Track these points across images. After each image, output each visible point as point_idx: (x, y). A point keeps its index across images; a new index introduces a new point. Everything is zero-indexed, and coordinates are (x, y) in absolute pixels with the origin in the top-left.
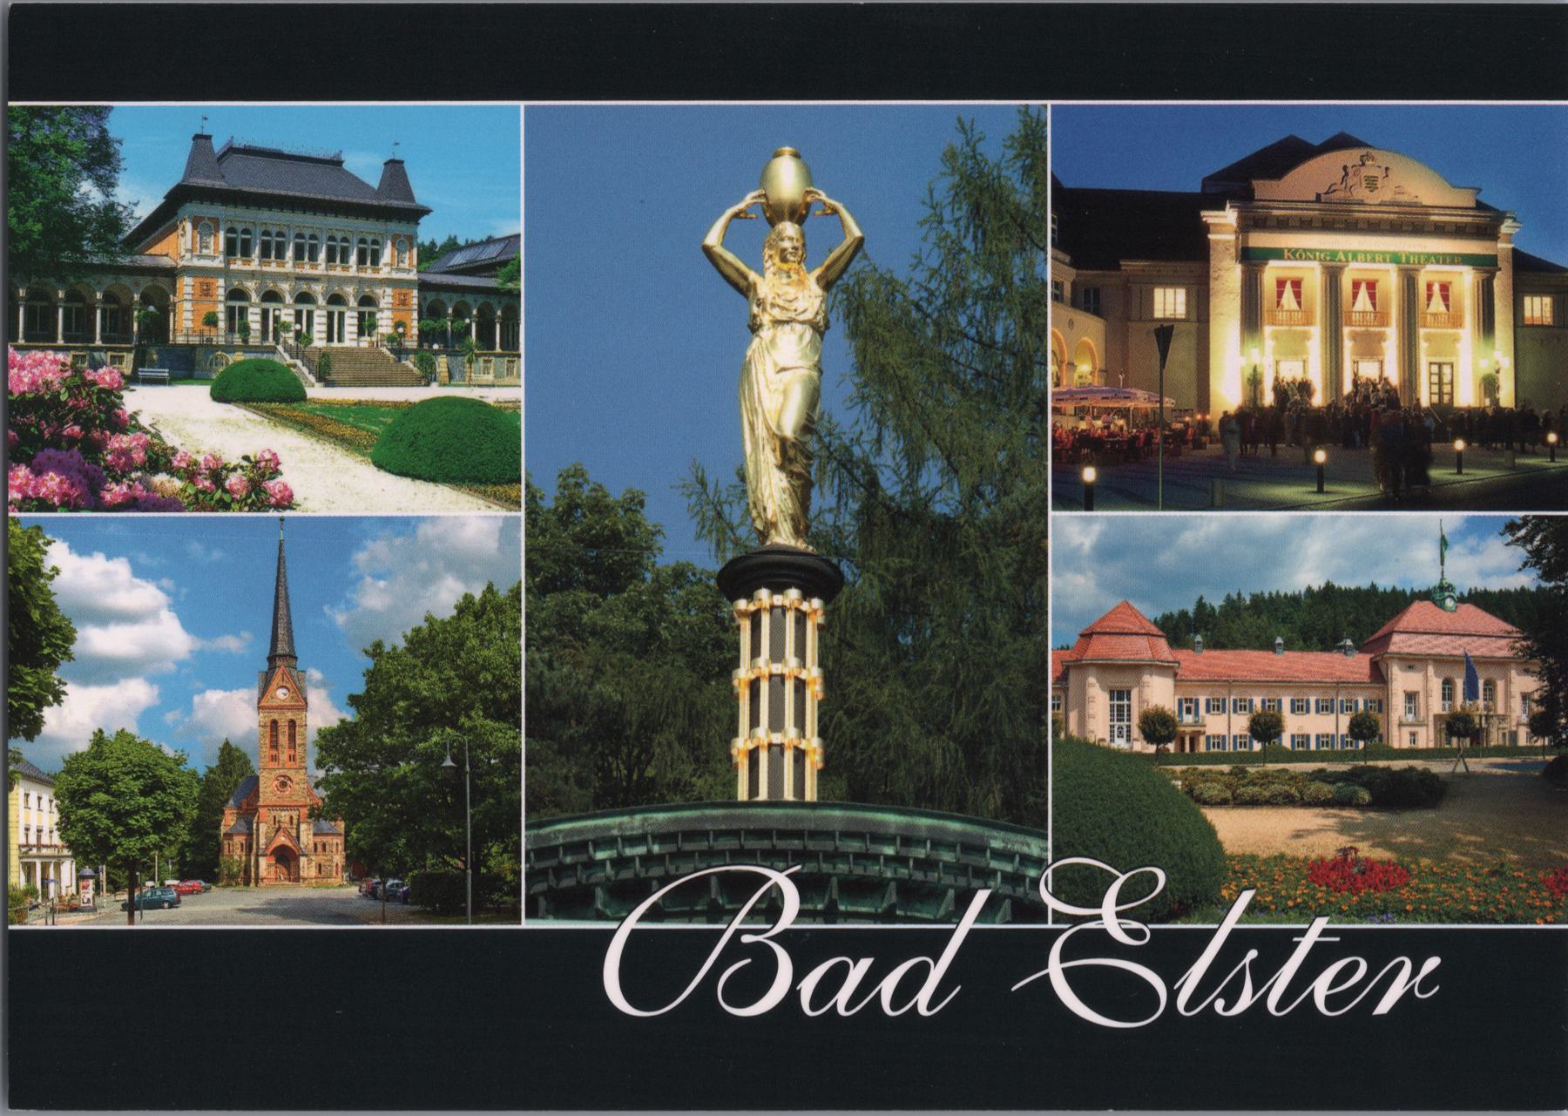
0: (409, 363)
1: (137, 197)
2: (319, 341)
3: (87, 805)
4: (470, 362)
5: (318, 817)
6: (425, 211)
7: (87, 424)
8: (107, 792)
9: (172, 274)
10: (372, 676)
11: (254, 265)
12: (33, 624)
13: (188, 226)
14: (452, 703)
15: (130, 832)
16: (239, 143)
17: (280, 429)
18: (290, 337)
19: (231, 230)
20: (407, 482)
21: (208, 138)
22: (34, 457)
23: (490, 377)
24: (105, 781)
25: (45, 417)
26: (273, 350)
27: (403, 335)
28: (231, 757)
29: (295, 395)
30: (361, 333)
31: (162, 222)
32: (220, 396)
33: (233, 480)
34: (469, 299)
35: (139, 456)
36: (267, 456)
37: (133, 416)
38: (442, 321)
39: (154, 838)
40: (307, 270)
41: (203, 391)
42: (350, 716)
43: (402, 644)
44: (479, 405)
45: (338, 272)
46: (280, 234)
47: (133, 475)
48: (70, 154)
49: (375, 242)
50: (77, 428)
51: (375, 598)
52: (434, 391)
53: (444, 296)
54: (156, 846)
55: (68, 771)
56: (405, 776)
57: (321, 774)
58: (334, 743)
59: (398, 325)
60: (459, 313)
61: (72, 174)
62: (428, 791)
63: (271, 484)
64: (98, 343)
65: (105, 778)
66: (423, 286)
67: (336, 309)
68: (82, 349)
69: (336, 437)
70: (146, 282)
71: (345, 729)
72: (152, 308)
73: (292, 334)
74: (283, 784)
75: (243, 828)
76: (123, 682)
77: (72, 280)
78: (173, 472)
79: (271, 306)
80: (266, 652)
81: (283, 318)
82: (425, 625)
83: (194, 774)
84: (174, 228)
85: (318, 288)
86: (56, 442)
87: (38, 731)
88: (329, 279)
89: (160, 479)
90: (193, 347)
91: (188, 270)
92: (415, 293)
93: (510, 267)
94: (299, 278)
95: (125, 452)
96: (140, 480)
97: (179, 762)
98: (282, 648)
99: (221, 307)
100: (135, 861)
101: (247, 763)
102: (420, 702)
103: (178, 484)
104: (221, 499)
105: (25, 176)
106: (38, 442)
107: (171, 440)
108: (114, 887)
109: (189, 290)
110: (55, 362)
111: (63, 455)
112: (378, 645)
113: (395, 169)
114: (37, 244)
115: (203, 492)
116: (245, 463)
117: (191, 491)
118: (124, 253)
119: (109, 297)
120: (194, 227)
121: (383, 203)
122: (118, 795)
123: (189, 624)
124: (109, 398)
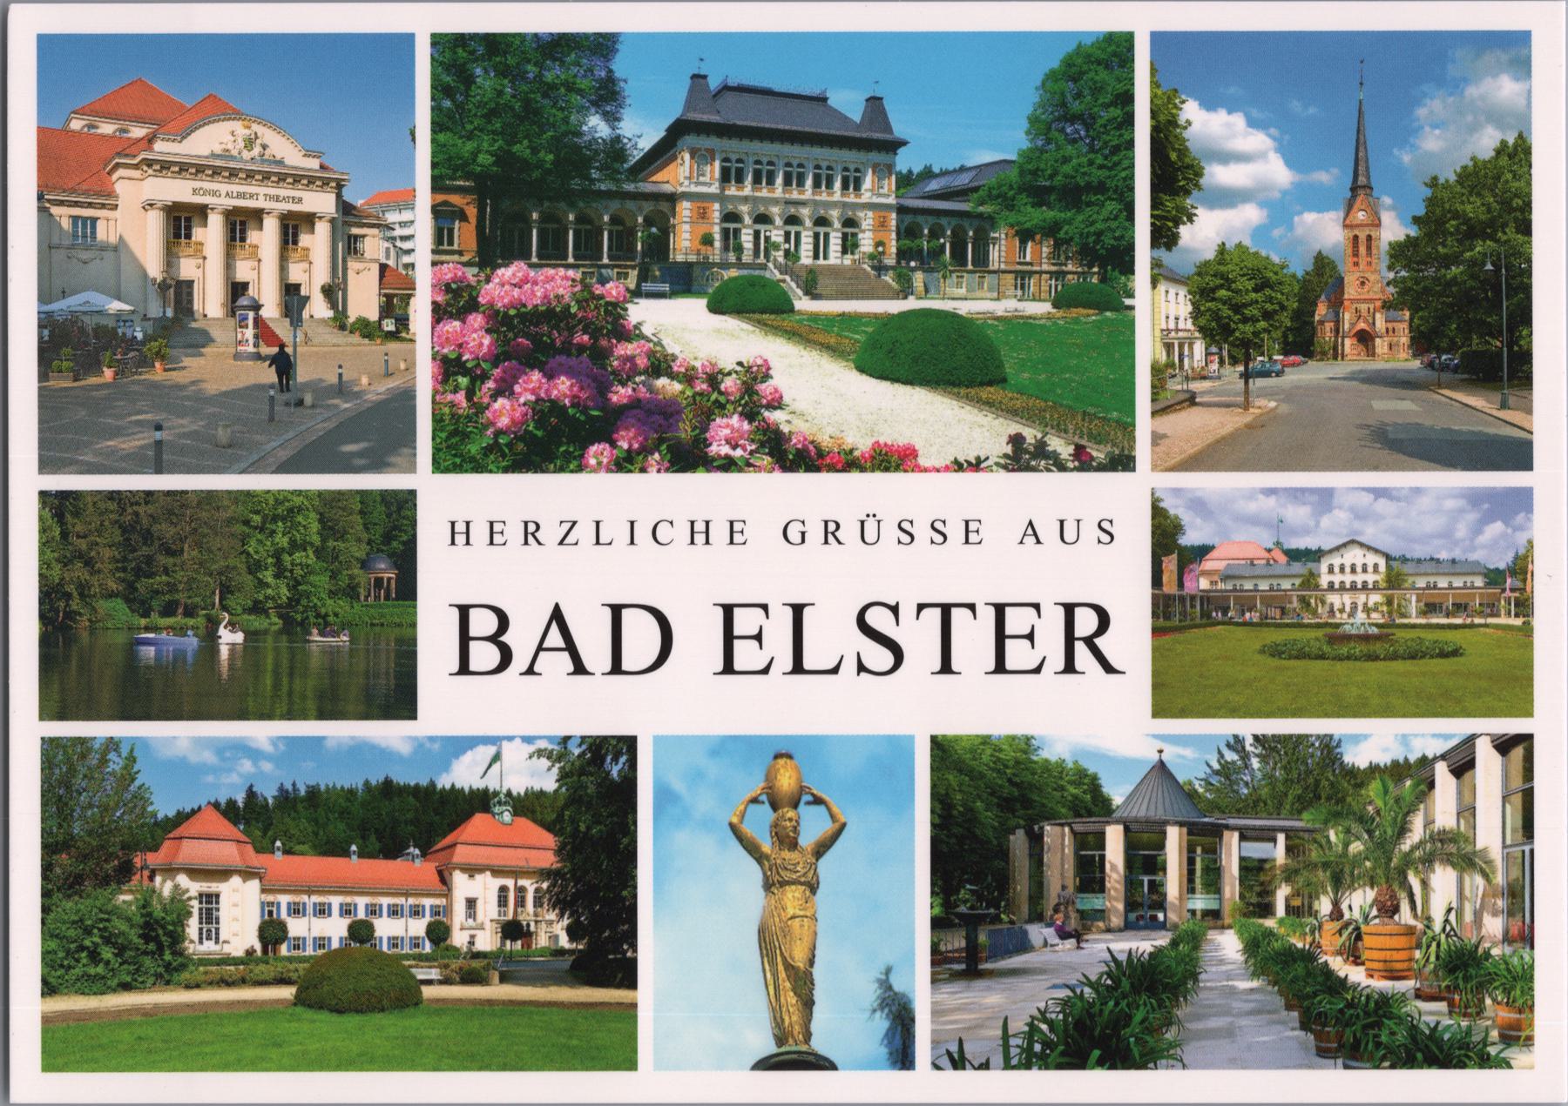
0: (888, 278)
1: (641, 130)
2: (806, 258)
3: (1214, 299)
4: (945, 277)
5: (1388, 309)
6: (903, 143)
7: (595, 334)
8: (1229, 289)
9: (672, 199)
10: (1431, 202)
11: (747, 190)
12: (1173, 163)
13: (687, 156)
14: (1492, 223)
15: (1245, 320)
16: (732, 82)
17: (770, 338)
18: (779, 256)
19: (726, 160)
20: (886, 385)
21: (705, 77)
22: (545, 363)
23: (962, 291)
24: (1227, 282)
25: (556, 327)
26: (764, 267)
27: (883, 253)
28: (1322, 263)
29: (783, 306)
30: (844, 251)
31: (662, 152)
32: (716, 308)
33: (729, 384)
34: (944, 221)
35: (642, 362)
36: (759, 362)
37: (637, 327)
38: (917, 242)
39: (1262, 324)
40: (795, 195)
41: (700, 304)
42: (1413, 232)
43: (1453, 178)
44: (954, 316)
45: (824, 197)
46: (770, 163)
47: (637, 379)
48: (580, 92)
49: (857, 170)
50: (586, 338)
51: (1432, 142)
52: (911, 304)
53: (920, 219)
54: (1265, 330)
55: (1199, 274)
56: (1455, 277)
57: (1391, 275)
58: (1399, 252)
59: (878, 244)
60: (935, 234)
61: (582, 110)
62: (1473, 288)
63: (763, 386)
64: (606, 261)
65: (1227, 279)
66: (901, 210)
67: (822, 230)
68: (591, 266)
69: (822, 345)
70: (648, 207)
71: (1410, 243)
72: (654, 230)
73: (781, 253)
74: (1363, 283)
75: (1331, 316)
76: (1241, 207)
77: (581, 204)
78: (673, 376)
79: (762, 227)
80: (1349, 184)
81: (773, 239)
82: (1471, 164)
83: (1294, 276)
84: (674, 158)
85: (805, 212)
86: (567, 349)
87: (1175, 243)
88: (815, 203)
89: (662, 382)
90: (689, 265)
91: (687, 196)
92: (894, 215)
93: (981, 192)
94: (788, 202)
95: (631, 359)
96: (643, 383)
97: (1283, 267)
98: (1362, 180)
99: (717, 229)
100: (1250, 341)
101: (1335, 267)
102: (1467, 221)
103: (677, 387)
104: (717, 401)
105: (537, 112)
106: (551, 350)
107: (672, 347)
108: (1234, 361)
109: (687, 213)
110: (566, 278)
111: (573, 361)
112: (1435, 178)
113: (875, 102)
114: (549, 172)
115: (701, 394)
116: (739, 368)
117: (689, 393)
118: (628, 179)
119: (615, 220)
120: (692, 157)
121: (864, 136)
122: (1237, 292)
123: (1290, 163)
124: (615, 311)
